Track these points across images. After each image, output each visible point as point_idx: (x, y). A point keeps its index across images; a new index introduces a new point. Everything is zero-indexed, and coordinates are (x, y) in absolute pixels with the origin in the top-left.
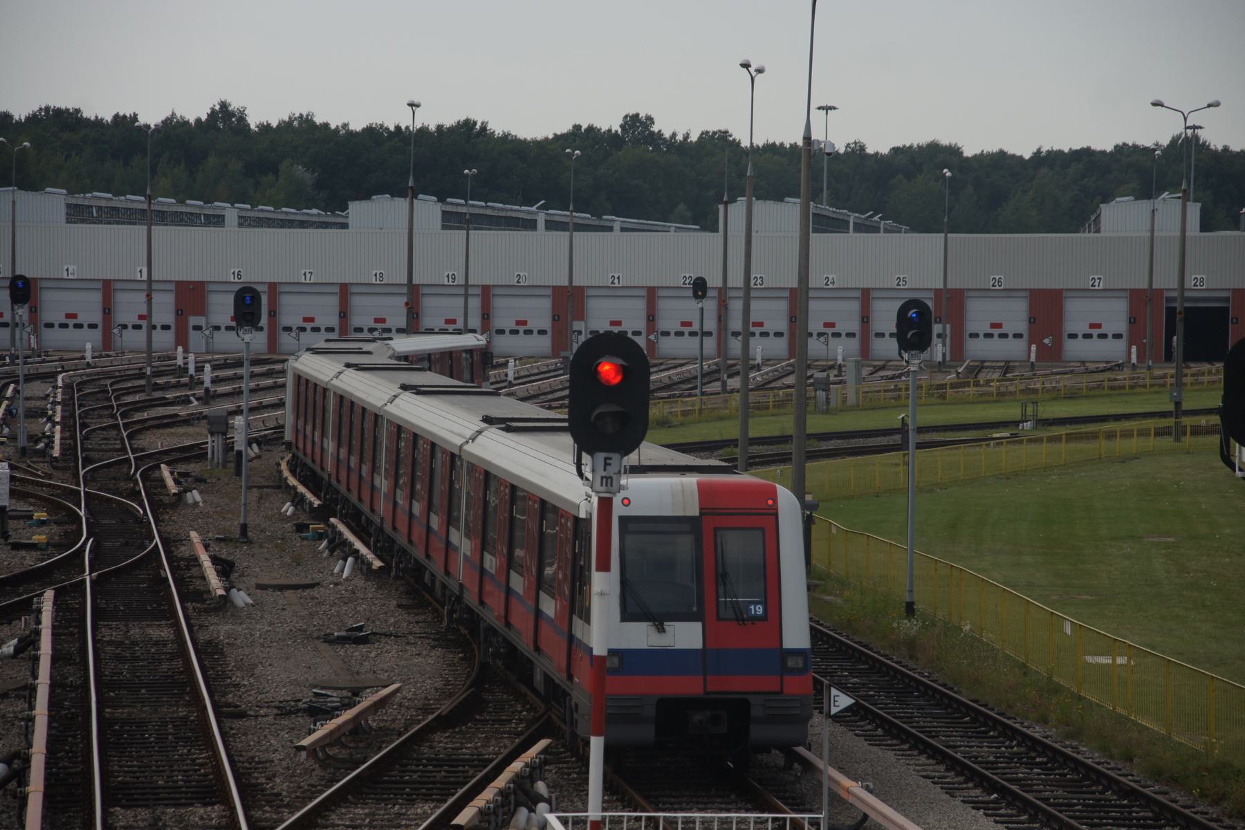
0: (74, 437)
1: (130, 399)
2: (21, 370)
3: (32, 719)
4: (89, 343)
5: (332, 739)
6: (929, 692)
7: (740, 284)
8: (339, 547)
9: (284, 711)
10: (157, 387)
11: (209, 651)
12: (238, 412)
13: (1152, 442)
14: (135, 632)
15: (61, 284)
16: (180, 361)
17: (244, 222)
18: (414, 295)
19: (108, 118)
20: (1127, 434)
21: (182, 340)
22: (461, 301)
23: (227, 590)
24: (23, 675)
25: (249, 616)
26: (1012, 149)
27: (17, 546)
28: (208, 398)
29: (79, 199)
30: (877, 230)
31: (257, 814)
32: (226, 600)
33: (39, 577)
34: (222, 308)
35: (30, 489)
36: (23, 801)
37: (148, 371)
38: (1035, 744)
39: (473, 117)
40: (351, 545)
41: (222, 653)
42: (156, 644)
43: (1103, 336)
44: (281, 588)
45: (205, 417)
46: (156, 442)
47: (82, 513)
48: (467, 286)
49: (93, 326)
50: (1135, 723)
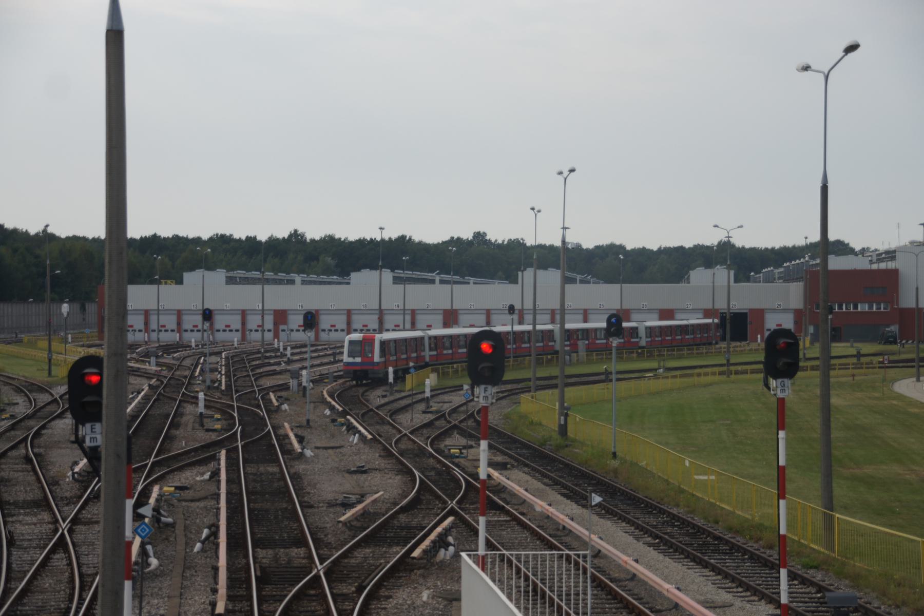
0: (230, 380)
1: (254, 363)
2: (207, 351)
3: (218, 509)
4: (236, 338)
5: (356, 518)
6: (623, 493)
7: (531, 307)
8: (351, 429)
9: (331, 505)
10: (267, 358)
11: (295, 477)
12: (306, 368)
13: (717, 378)
14: (262, 469)
15: (223, 312)
16: (276, 346)
17: (304, 282)
18: (381, 313)
19: (244, 238)
20: (706, 374)
21: (276, 336)
22: (402, 317)
23: (303, 449)
24: (212, 488)
25: (313, 461)
26: (648, 247)
27: (208, 430)
28: (289, 362)
29: (231, 274)
30: (589, 283)
31: (321, 552)
32: (301, 455)
33: (218, 444)
34: (296, 321)
35: (212, 404)
36: (217, 545)
37: (262, 350)
38: (674, 517)
39: (405, 233)
40: (357, 428)
41: (301, 478)
42: (272, 474)
43: (231, 331)
44: (326, 448)
45: (289, 371)
46: (267, 382)
47: (236, 415)
48: (404, 310)
49: (237, 331)
50: (719, 506)
